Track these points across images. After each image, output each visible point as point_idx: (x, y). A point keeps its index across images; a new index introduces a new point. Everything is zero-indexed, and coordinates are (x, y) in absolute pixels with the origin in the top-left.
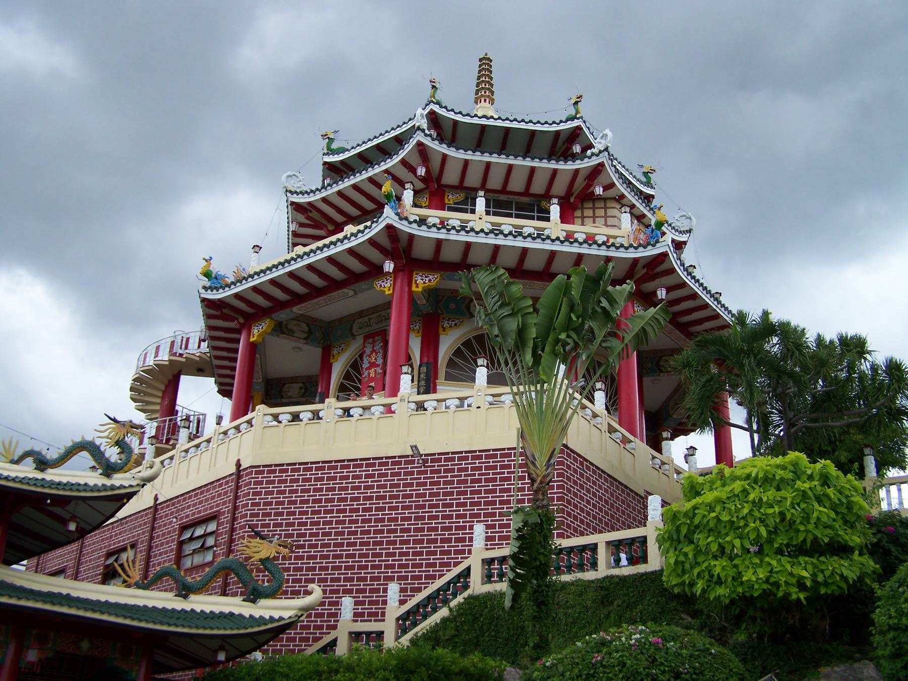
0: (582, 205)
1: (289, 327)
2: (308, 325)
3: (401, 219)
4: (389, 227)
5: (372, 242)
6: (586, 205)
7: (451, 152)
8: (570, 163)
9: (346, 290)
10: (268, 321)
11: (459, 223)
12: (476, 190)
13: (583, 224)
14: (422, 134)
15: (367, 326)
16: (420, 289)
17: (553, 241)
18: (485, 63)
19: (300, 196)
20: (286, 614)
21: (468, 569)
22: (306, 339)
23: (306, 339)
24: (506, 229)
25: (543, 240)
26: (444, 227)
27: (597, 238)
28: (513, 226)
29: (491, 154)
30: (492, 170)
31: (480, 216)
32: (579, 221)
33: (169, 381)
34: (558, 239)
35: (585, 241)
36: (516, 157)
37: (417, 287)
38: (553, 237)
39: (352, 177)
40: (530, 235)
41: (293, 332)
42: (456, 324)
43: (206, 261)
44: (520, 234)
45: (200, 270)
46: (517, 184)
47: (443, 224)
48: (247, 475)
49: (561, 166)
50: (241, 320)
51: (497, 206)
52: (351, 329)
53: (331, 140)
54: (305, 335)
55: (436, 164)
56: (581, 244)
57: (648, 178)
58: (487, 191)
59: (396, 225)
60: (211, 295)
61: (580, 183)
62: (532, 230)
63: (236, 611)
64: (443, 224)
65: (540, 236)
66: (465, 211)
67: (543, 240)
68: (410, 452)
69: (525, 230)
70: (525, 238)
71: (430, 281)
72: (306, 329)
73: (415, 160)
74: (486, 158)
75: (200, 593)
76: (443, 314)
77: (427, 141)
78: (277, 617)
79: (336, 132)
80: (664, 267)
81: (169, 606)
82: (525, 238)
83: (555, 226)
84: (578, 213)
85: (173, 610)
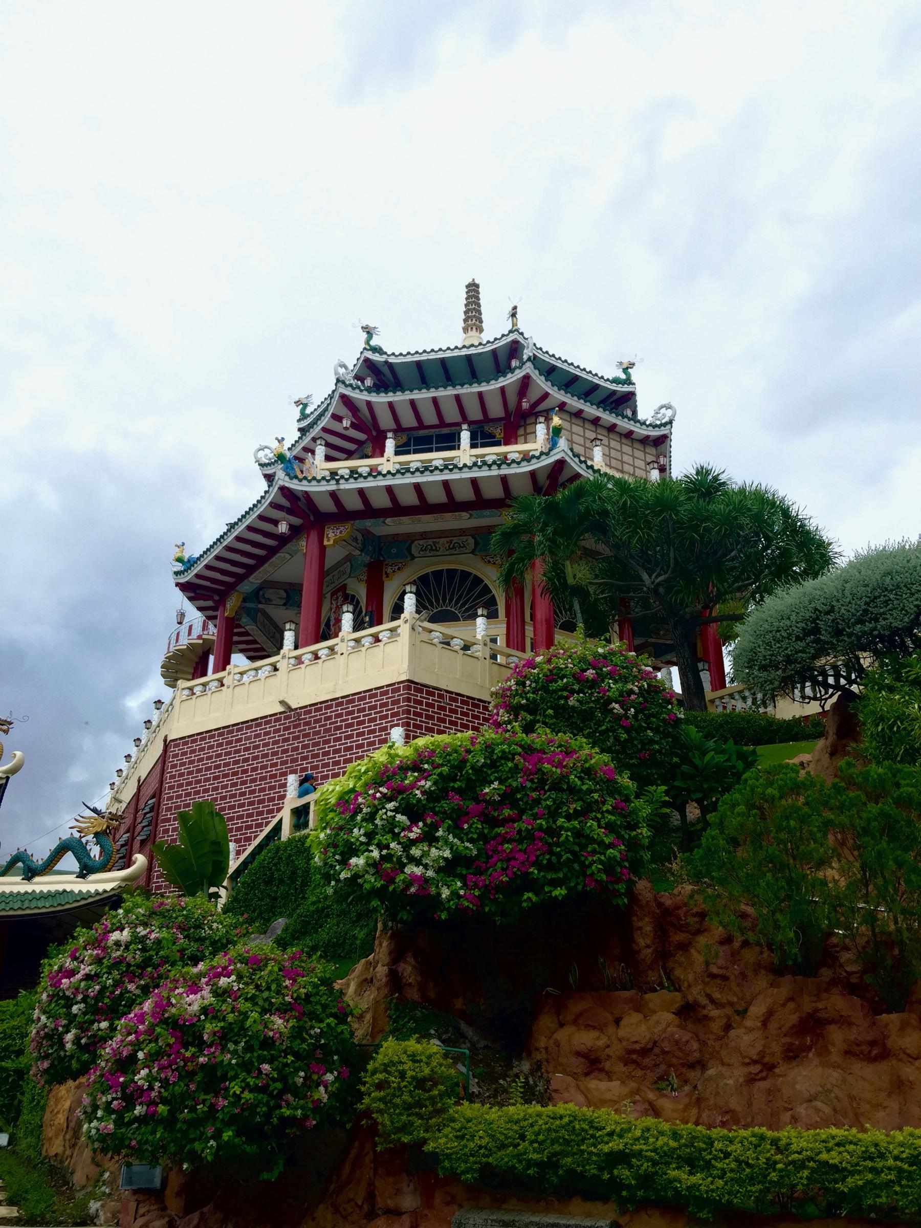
0: (525, 421)
1: (266, 596)
2: (286, 591)
3: (291, 479)
4: (282, 489)
5: (274, 505)
6: (528, 421)
7: (484, 388)
8: (399, 393)
9: (464, 514)
10: (235, 595)
11: (441, 462)
12: (458, 425)
13: (526, 442)
14: (343, 386)
15: (432, 550)
16: (331, 542)
17: (319, 481)
18: (473, 289)
19: (662, 428)
20: (109, 886)
21: (281, 820)
22: (284, 605)
23: (284, 605)
24: (364, 471)
25: (432, 471)
26: (333, 478)
27: (360, 470)
28: (421, 461)
29: (411, 391)
30: (487, 399)
31: (389, 459)
32: (521, 439)
33: (197, 664)
34: (323, 478)
35: (370, 474)
36: (488, 382)
37: (328, 540)
38: (319, 478)
39: (607, 412)
40: (417, 470)
41: (269, 600)
42: (399, 569)
43: (279, 441)
44: (408, 470)
45: (173, 558)
46: (496, 410)
47: (354, 473)
48: (175, 746)
49: (502, 382)
50: (217, 598)
51: (481, 438)
52: (409, 550)
53: (305, 406)
54: (283, 601)
55: (365, 410)
56: (365, 478)
57: (629, 376)
58: (470, 423)
59: (287, 485)
60: (183, 579)
61: (512, 399)
62: (419, 464)
63: (68, 888)
64: (354, 473)
65: (374, 472)
66: (454, 449)
67: (432, 471)
68: (282, 709)
69: (412, 465)
70: (413, 473)
71: (341, 532)
72: (284, 595)
73: (344, 411)
74: (433, 393)
75: (44, 875)
76: (385, 560)
77: (348, 392)
78: (101, 890)
79: (308, 397)
80: (565, 475)
81: (15, 889)
82: (413, 473)
83: (465, 453)
84: (521, 431)
85: (19, 893)
